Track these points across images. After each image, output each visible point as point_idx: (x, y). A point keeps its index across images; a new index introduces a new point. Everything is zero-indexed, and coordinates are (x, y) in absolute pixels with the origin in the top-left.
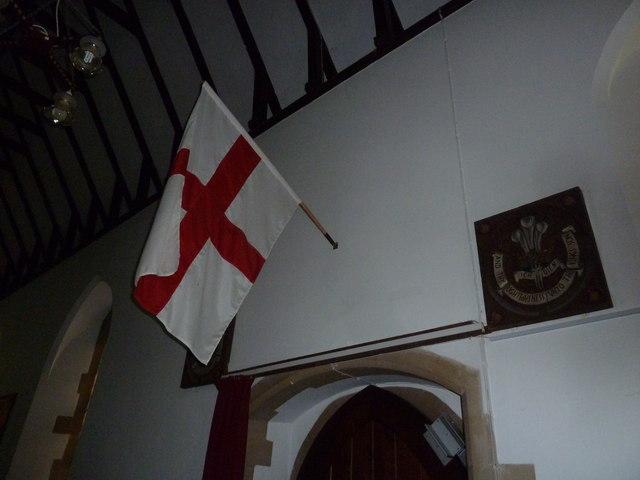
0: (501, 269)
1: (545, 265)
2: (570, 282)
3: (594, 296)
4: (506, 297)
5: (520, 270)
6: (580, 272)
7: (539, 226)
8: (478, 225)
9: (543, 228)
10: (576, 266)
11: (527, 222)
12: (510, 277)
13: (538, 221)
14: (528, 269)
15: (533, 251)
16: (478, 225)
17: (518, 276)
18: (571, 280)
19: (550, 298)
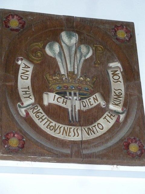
0: (28, 82)
1: (83, 96)
2: (111, 125)
3: (122, 34)
4: (28, 120)
5: (51, 91)
6: (122, 117)
7: (84, 49)
8: (129, 27)
9: (87, 52)
10: (119, 109)
11: (70, 37)
12: (39, 100)
13: (81, 41)
14: (62, 94)
15: (71, 74)
16: (129, 27)
17: (50, 98)
18: (112, 122)
19: (86, 137)
